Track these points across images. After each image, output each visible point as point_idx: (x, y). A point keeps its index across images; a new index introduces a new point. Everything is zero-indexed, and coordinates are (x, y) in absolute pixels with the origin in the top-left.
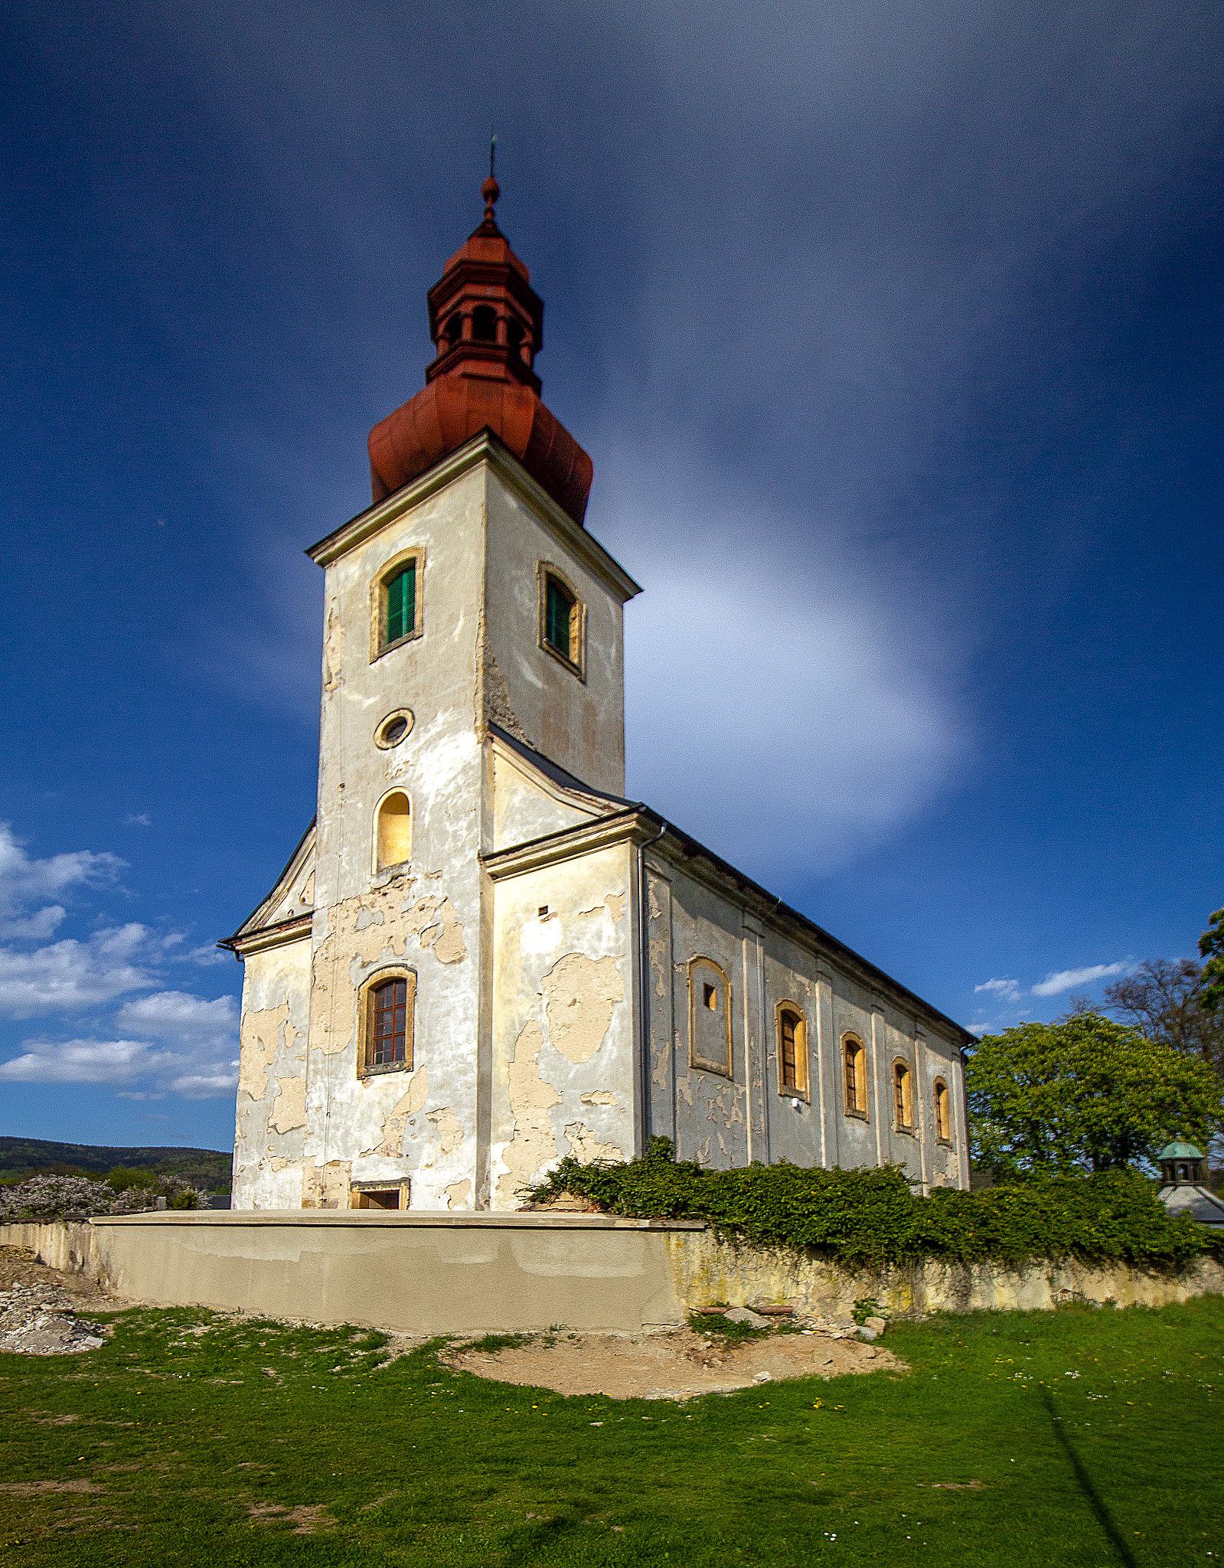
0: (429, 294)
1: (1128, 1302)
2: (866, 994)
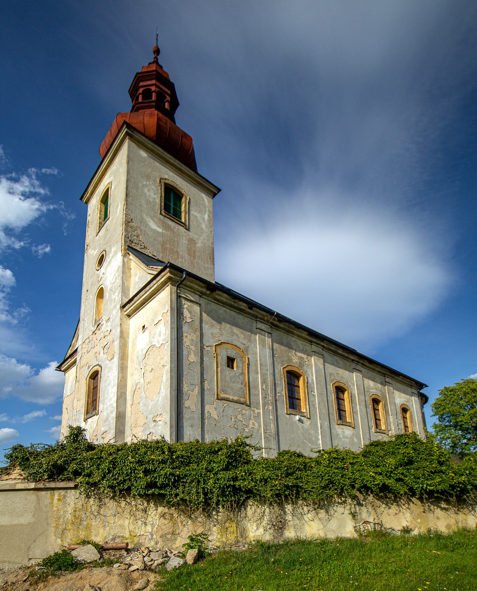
0: (129, 91)
1: (423, 530)
2: (348, 363)
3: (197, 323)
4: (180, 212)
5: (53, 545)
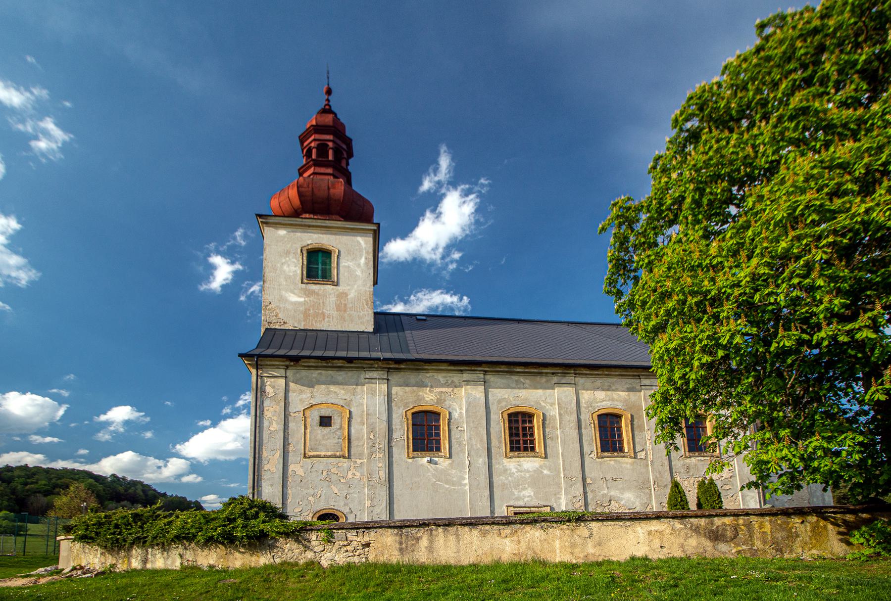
2: (544, 379)
3: (281, 394)
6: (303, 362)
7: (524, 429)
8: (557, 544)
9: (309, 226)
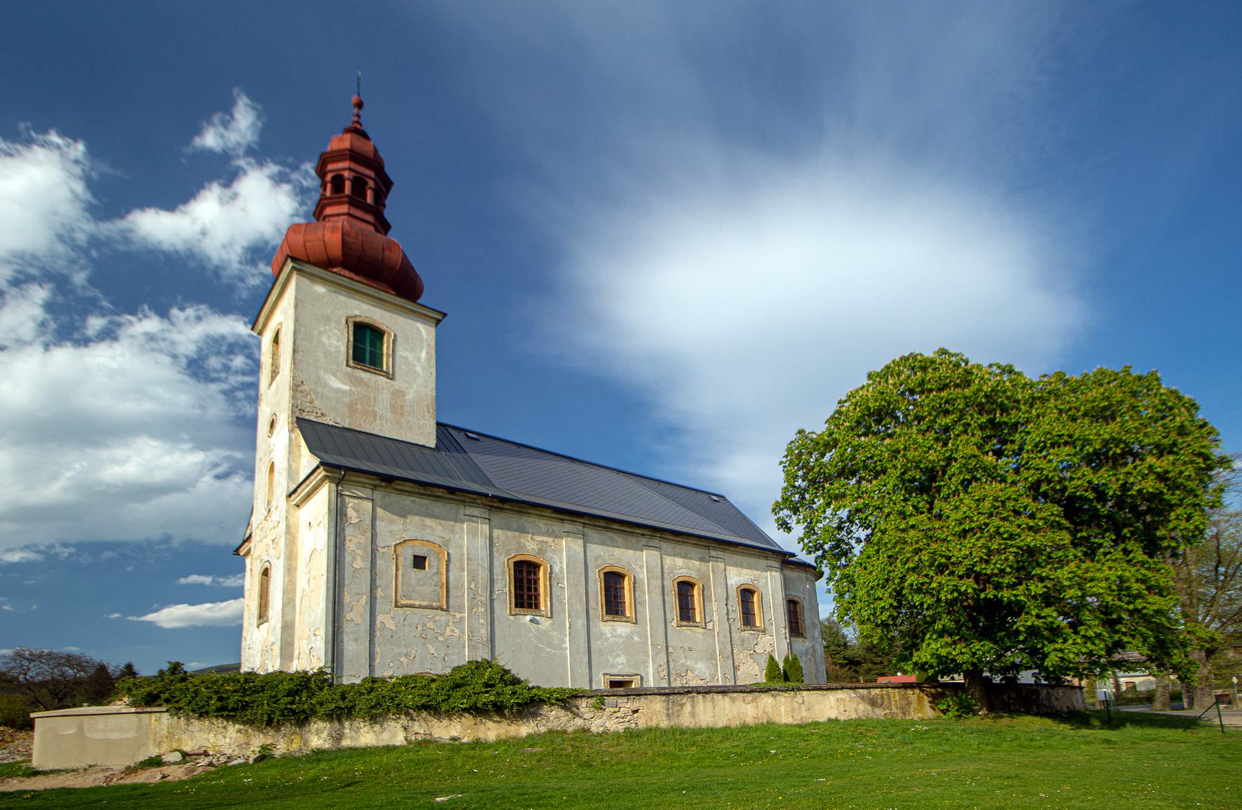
2: (634, 540)
3: (368, 522)
4: (382, 355)
5: (153, 752)
6: (396, 485)
7: (529, 581)
8: (782, 709)
9: (358, 292)
